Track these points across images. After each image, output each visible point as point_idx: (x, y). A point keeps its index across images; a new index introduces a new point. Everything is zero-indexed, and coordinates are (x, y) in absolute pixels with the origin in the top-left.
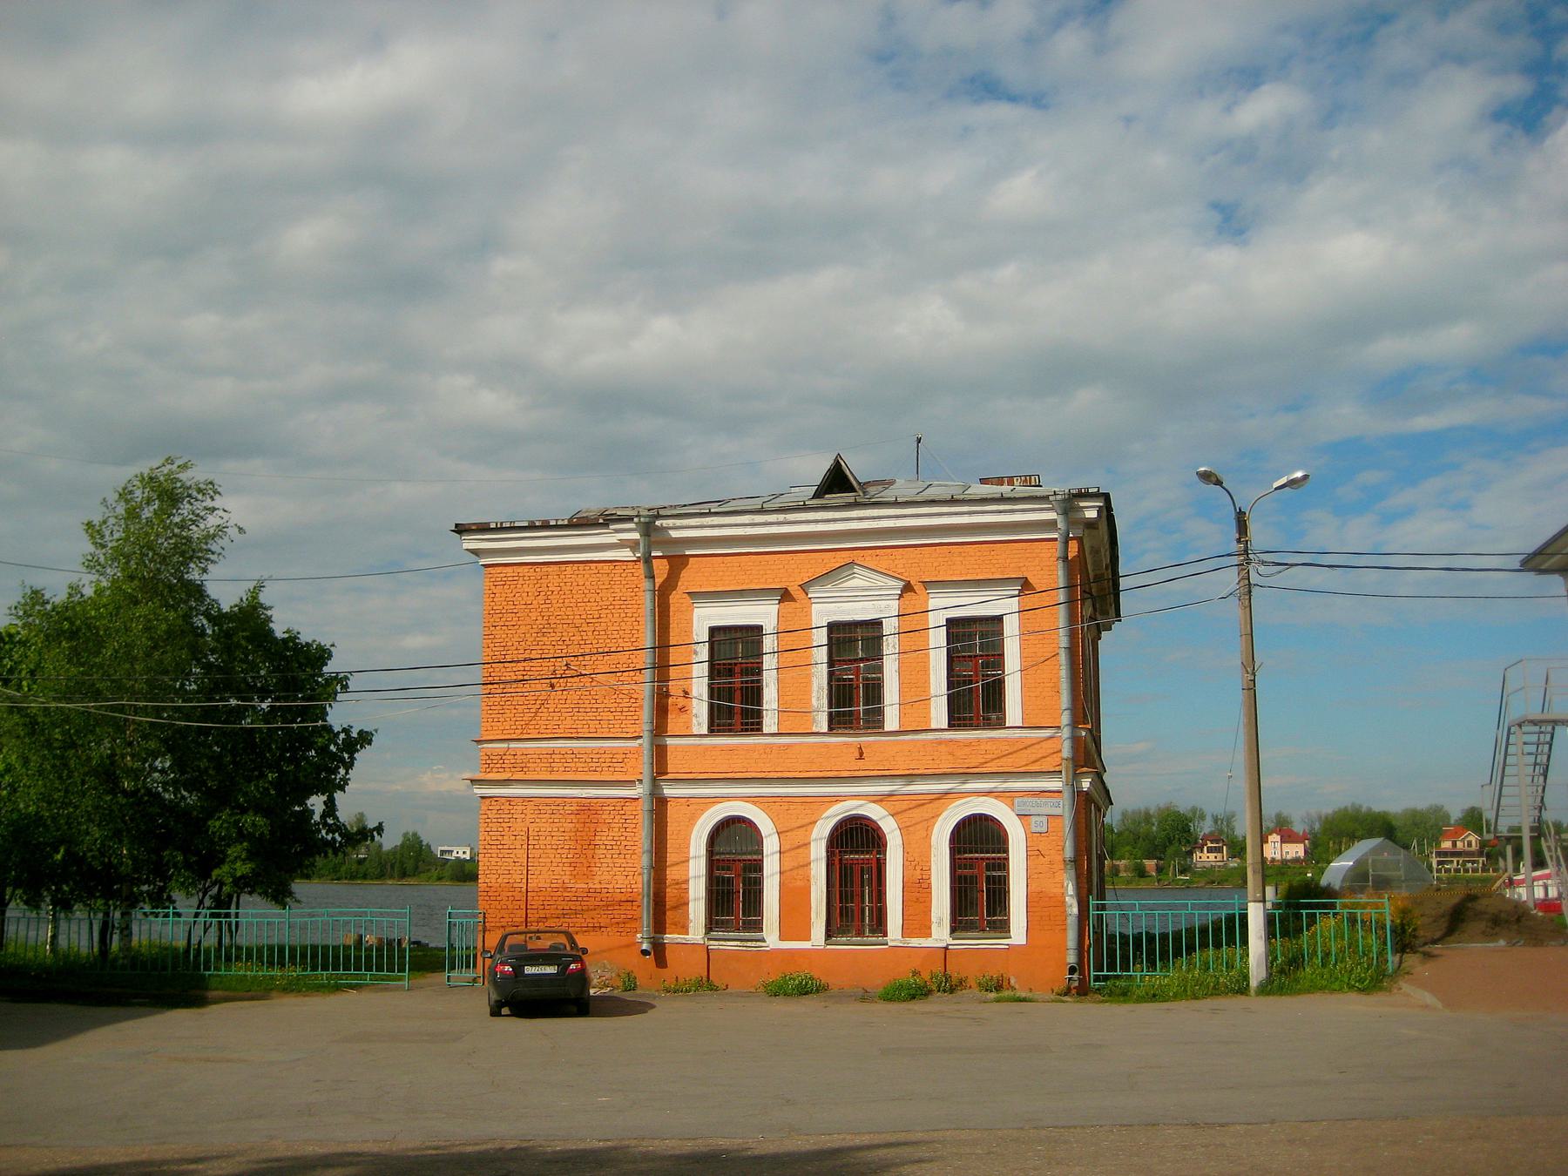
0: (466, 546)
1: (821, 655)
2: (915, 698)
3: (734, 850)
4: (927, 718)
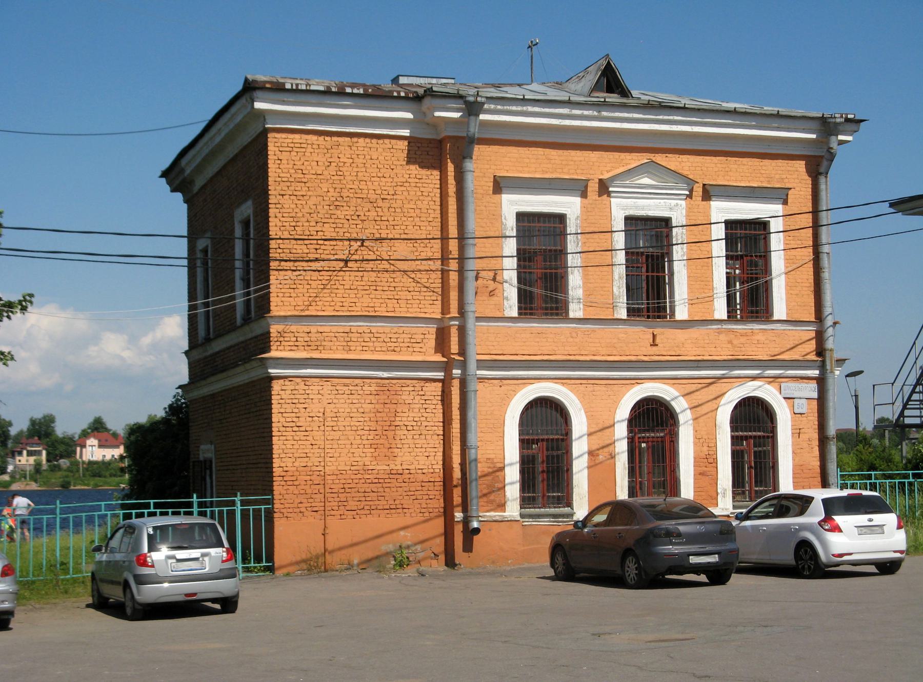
2: (700, 297)
3: (546, 427)
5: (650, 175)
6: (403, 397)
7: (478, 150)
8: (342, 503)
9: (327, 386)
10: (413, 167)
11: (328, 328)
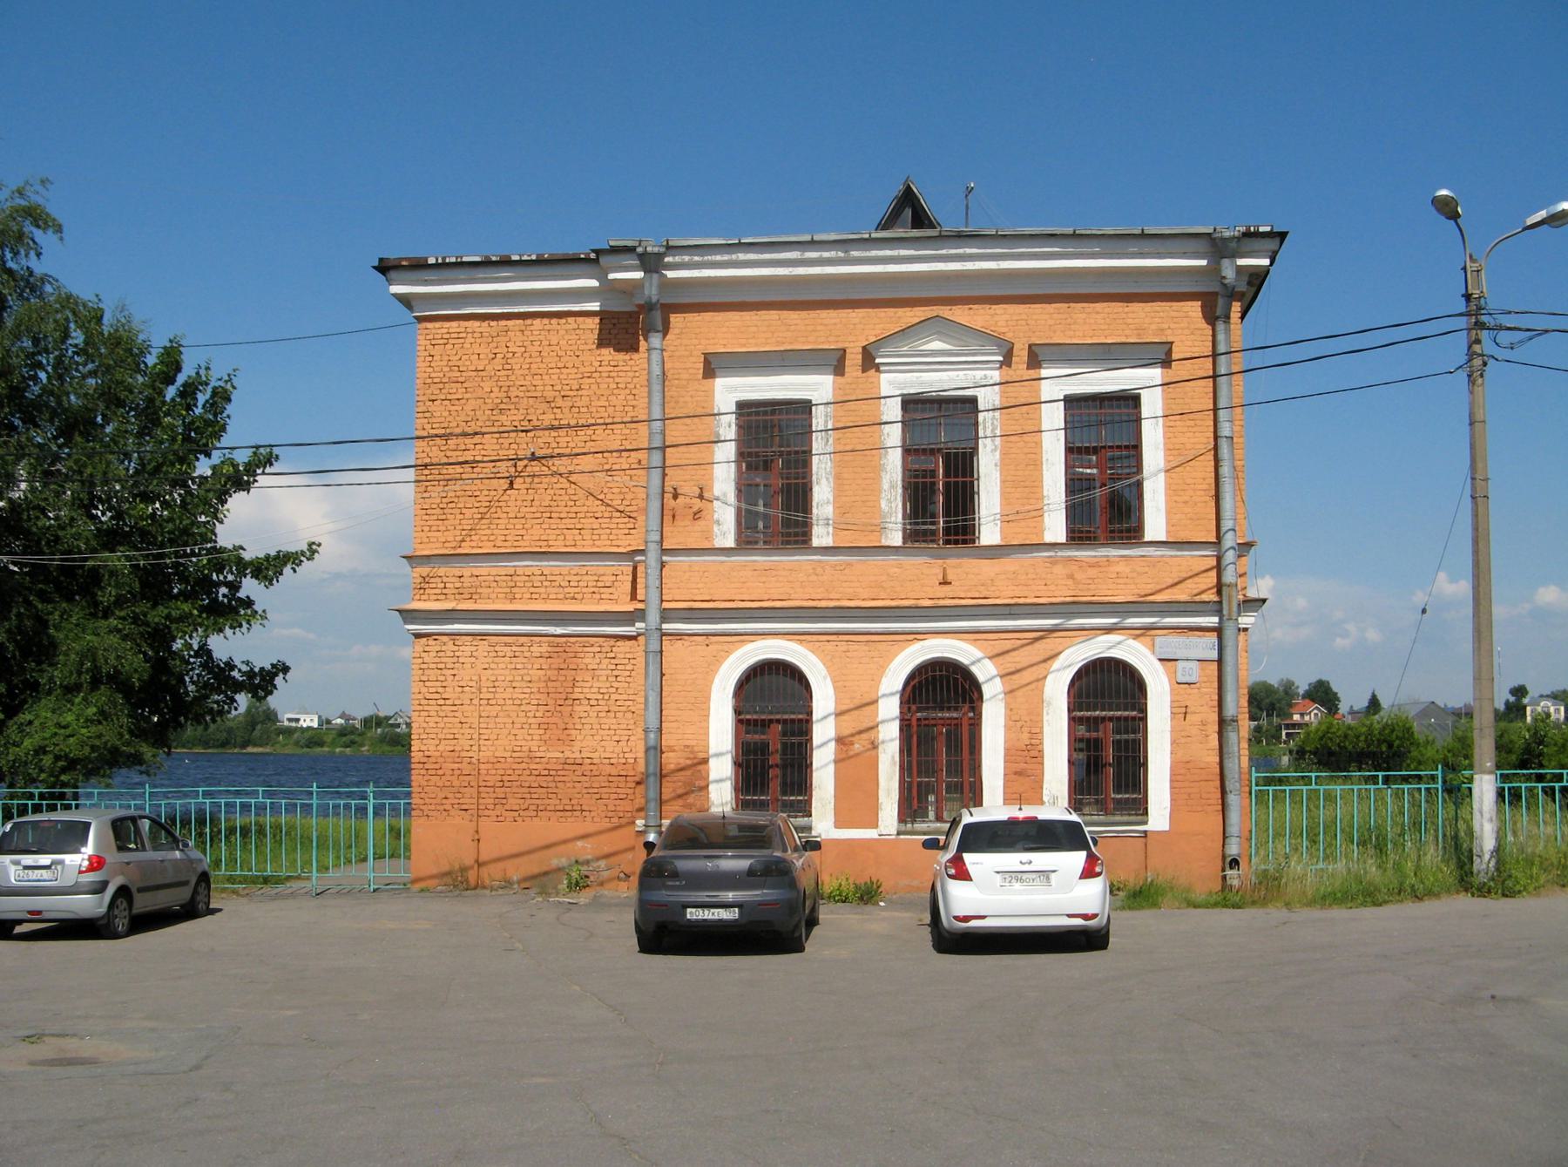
0: (395, 289)
1: (893, 435)
4: (1041, 531)
5: (942, 335)
6: (586, 661)
7: (676, 320)
8: (501, 801)
9: (483, 646)
10: (605, 351)
11: (484, 569)
